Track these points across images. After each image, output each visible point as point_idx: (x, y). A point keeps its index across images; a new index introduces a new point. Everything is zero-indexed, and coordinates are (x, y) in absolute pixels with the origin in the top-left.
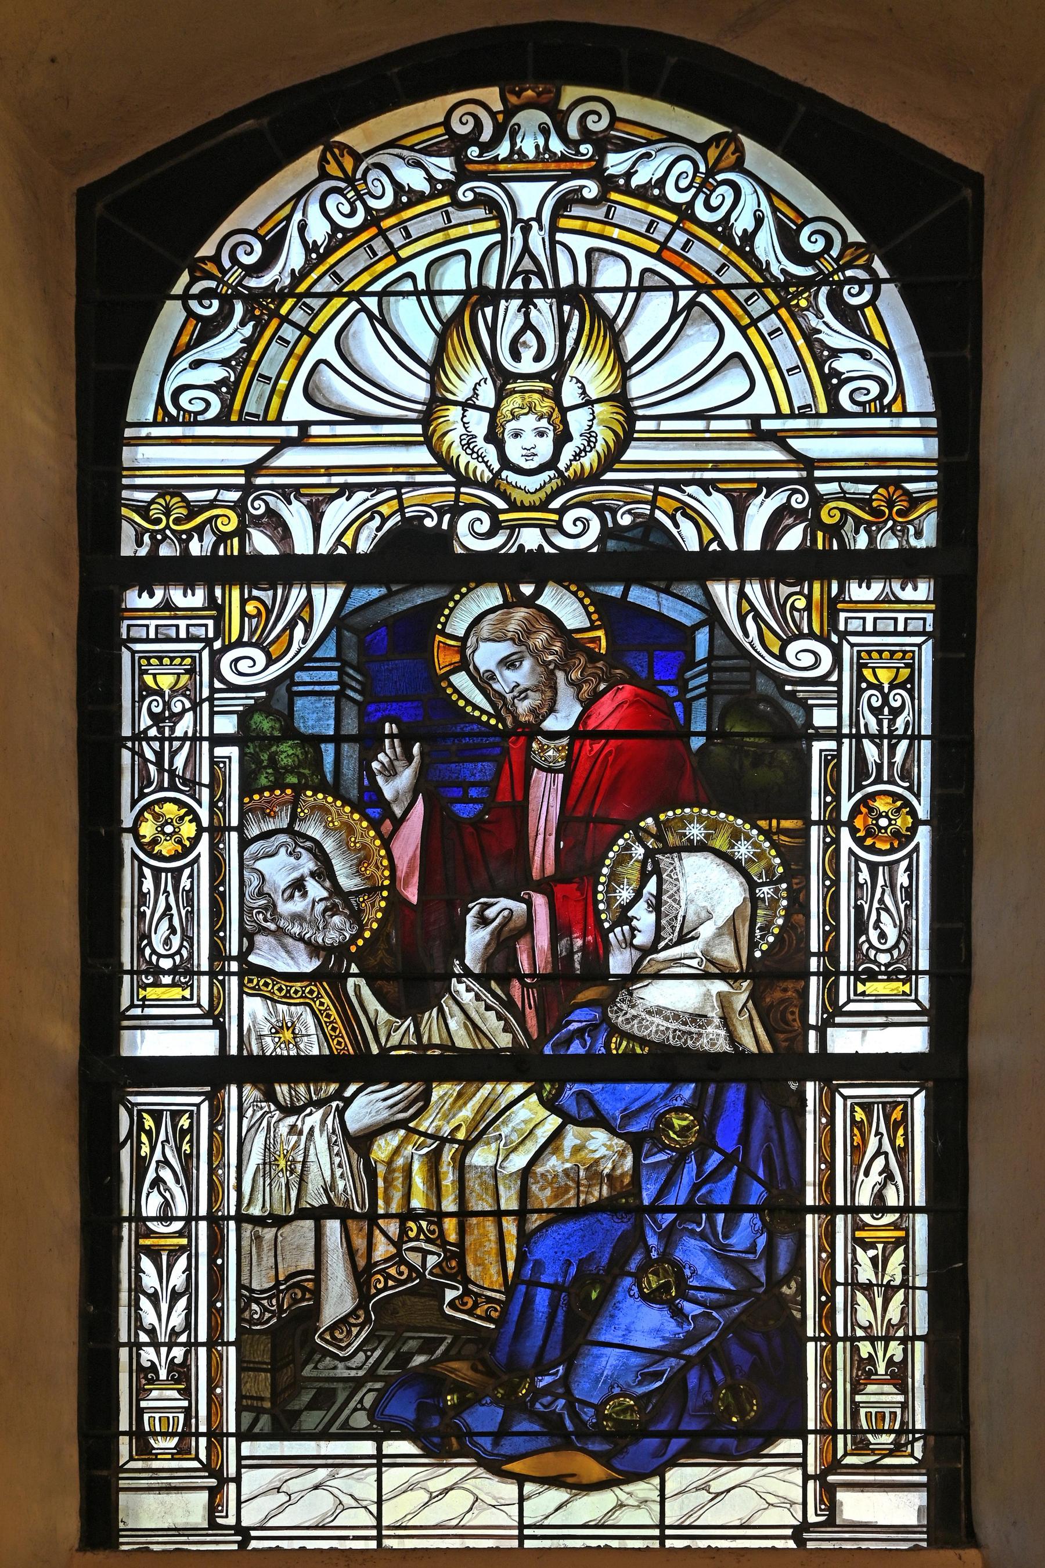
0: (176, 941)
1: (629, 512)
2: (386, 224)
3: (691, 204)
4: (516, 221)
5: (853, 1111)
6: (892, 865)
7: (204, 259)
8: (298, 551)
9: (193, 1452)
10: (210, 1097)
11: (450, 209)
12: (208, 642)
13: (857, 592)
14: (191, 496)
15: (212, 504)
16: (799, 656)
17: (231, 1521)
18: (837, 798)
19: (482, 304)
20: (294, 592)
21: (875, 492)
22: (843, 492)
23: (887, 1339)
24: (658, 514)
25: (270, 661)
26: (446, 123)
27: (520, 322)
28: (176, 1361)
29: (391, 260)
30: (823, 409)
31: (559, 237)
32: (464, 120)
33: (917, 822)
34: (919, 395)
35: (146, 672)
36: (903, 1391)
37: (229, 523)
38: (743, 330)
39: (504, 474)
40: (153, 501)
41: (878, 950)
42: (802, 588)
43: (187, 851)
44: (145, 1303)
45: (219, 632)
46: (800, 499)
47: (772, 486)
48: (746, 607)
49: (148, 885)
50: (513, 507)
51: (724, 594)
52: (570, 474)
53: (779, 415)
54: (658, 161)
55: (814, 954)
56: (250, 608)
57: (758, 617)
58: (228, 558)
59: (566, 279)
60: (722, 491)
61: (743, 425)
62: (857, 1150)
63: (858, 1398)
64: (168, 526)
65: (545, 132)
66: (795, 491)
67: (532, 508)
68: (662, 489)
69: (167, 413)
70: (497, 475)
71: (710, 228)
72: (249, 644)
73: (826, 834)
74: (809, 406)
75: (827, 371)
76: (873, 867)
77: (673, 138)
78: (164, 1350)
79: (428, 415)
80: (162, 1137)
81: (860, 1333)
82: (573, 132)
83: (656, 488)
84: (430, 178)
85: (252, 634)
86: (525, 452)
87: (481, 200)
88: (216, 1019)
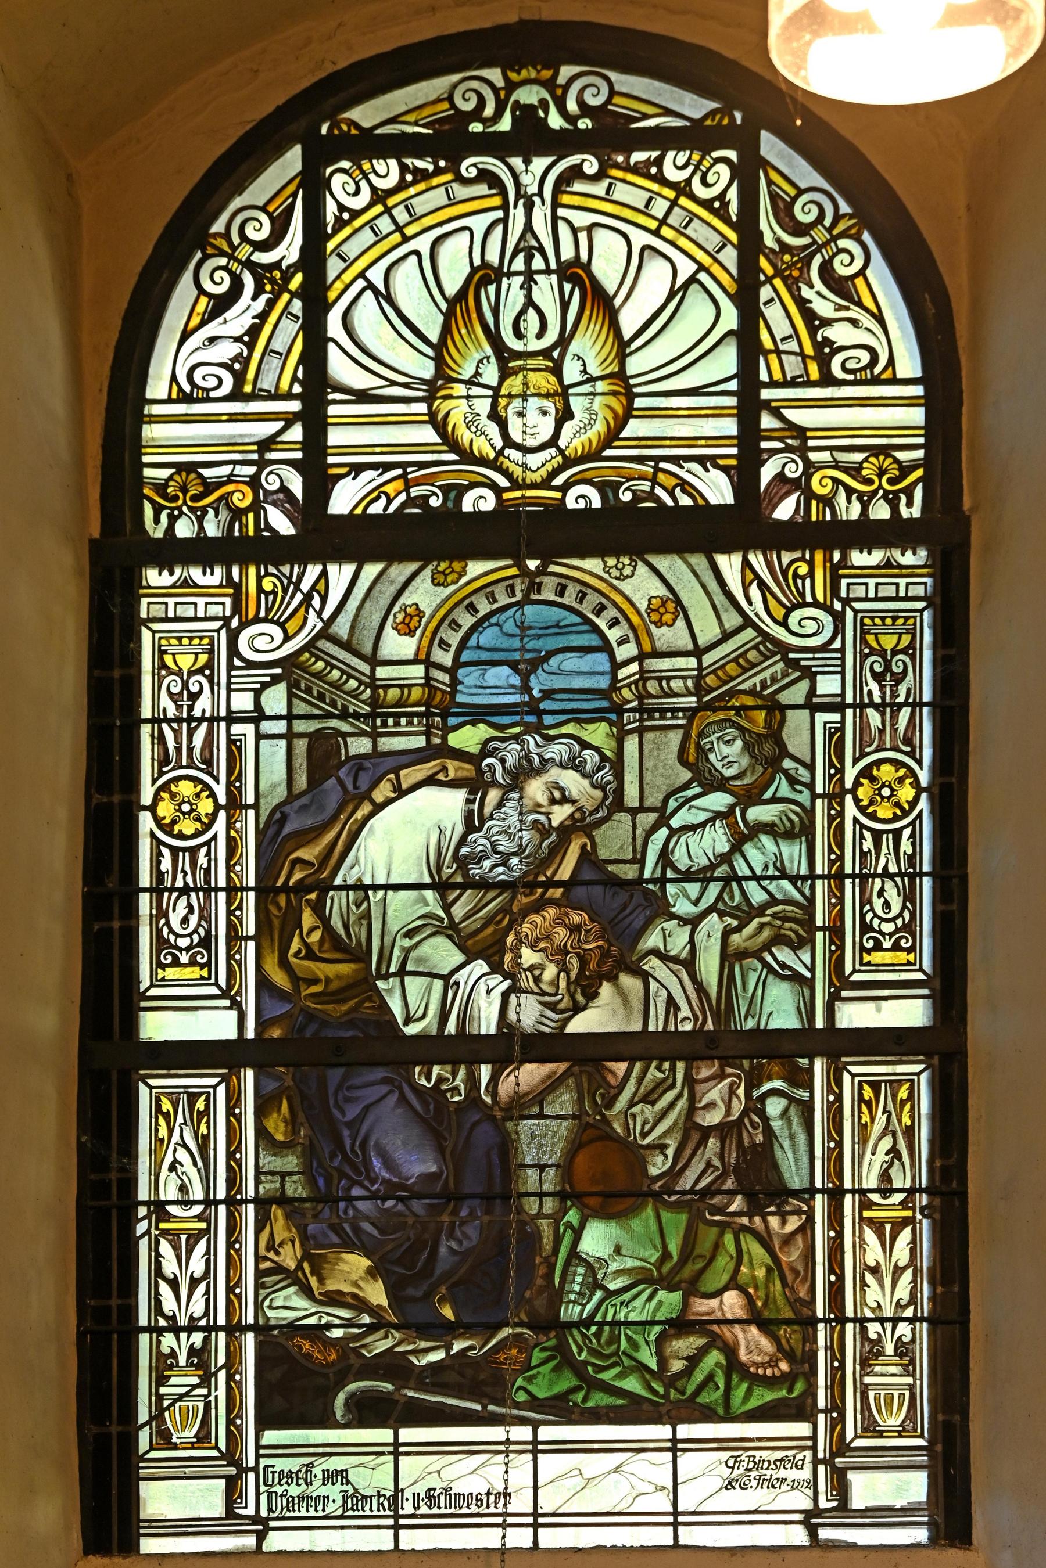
0: (194, 919)
2: (391, 202)
3: (688, 181)
4: (518, 195)
5: (861, 1088)
6: (897, 834)
7: (216, 235)
9: (213, 1441)
10: (224, 1078)
11: (454, 185)
13: (858, 558)
14: (206, 472)
15: (230, 479)
16: (803, 623)
17: (251, 1511)
18: (841, 771)
19: (485, 281)
20: (310, 567)
21: (866, 460)
22: (835, 460)
23: (895, 1321)
24: (658, 491)
25: (287, 638)
27: (521, 300)
31: (561, 212)
33: (152, 809)
35: (165, 652)
37: (242, 499)
39: (507, 452)
40: (171, 478)
41: (882, 920)
42: (804, 555)
43: (208, 827)
44: (164, 1289)
45: (237, 608)
48: (750, 576)
49: (166, 864)
50: (516, 485)
55: (820, 929)
56: (267, 584)
57: (762, 586)
59: (567, 253)
63: (868, 1380)
67: (534, 486)
68: (662, 465)
69: (180, 389)
70: (500, 453)
71: (707, 204)
72: (265, 620)
73: (831, 807)
75: (819, 339)
76: (877, 835)
78: (183, 1336)
79: (433, 389)
80: (180, 1119)
81: (869, 1314)
82: (572, 106)
83: (657, 464)
85: (268, 610)
87: (485, 176)
88: (233, 1000)
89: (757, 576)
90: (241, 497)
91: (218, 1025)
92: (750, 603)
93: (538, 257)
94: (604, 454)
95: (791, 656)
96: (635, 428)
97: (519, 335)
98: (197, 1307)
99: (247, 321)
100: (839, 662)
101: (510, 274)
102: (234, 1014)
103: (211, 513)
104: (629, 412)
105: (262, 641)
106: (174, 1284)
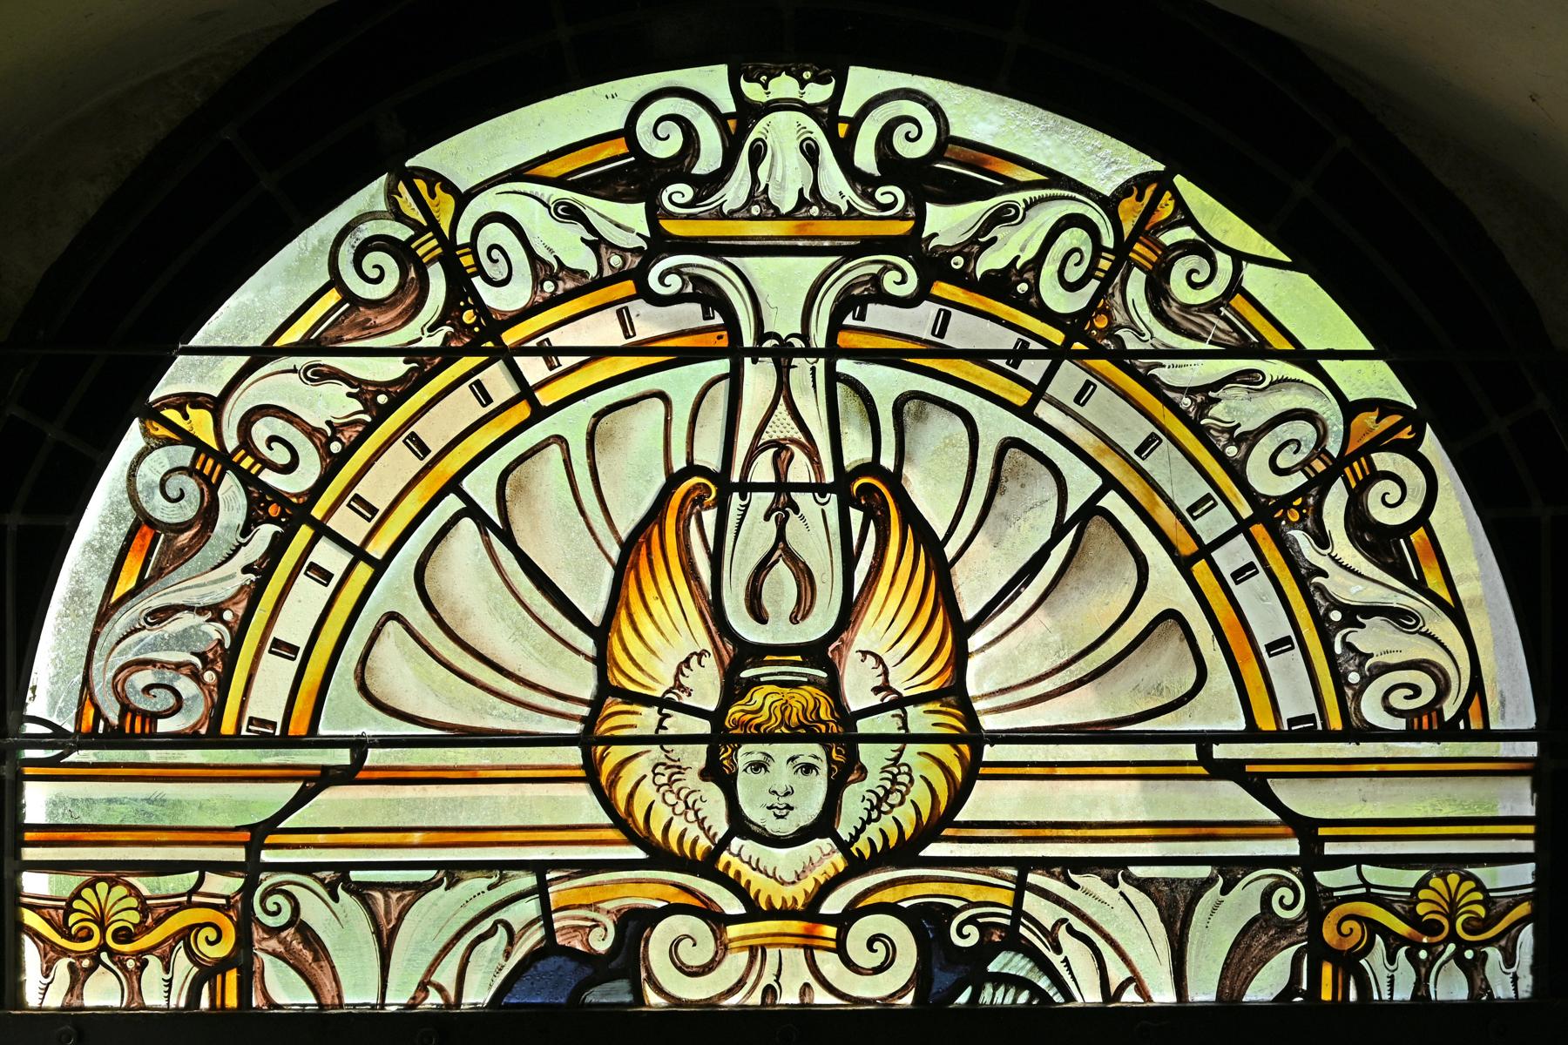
15: (189, 901)
21: (1423, 884)
26: (628, 132)
29: (523, 411)
30: (1336, 723)
38: (1184, 565)
47: (1231, 870)
50: (754, 912)
52: (862, 845)
53: (1252, 734)
58: (219, 1013)
59: (856, 450)
60: (1142, 885)
61: (1189, 752)
64: (103, 947)
66: (1282, 882)
68: (1032, 878)
74: (1311, 718)
82: (865, 157)
84: (597, 244)
86: (773, 800)
93: (800, 458)
94: (924, 853)
97: (759, 616)
101: (746, 488)
103: (154, 963)
104: (974, 770)
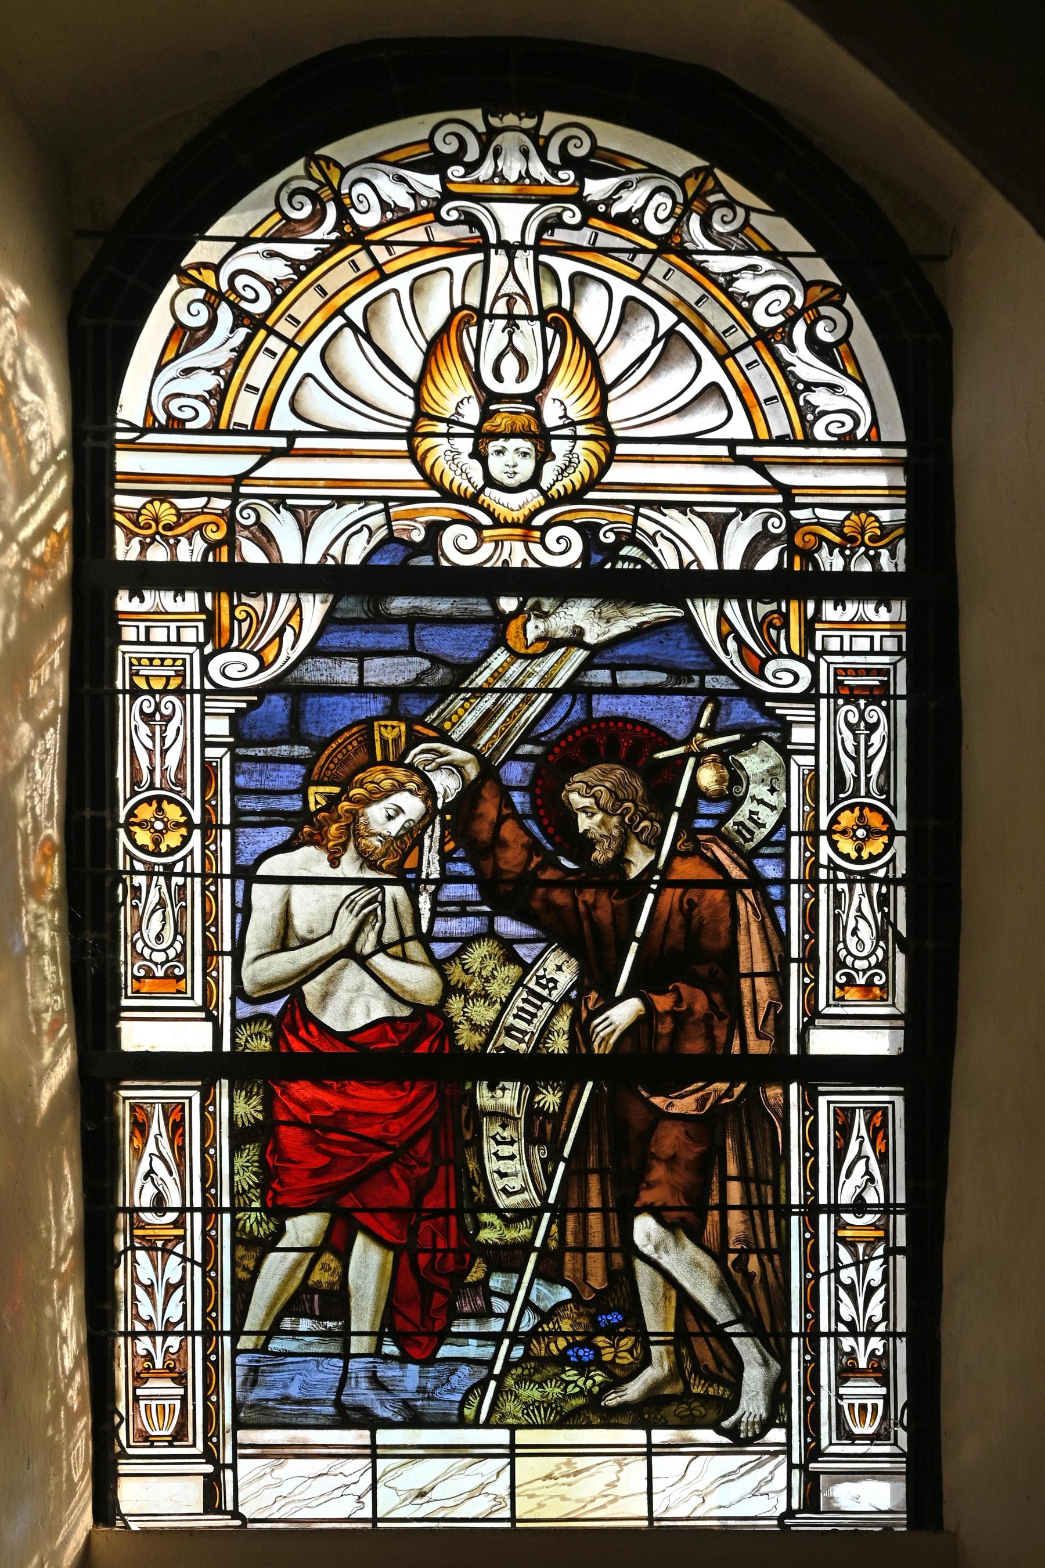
1: (611, 530)
8: (286, 560)
12: (200, 646)
14: (182, 503)
19: (466, 322)
20: (284, 597)
21: (847, 518)
25: (263, 668)
28: (171, 1350)
29: (376, 276)
32: (447, 140)
34: (894, 429)
36: (885, 1383)
38: (721, 360)
41: (856, 958)
42: (779, 606)
45: (209, 635)
46: (777, 524)
50: (497, 524)
51: (705, 615)
53: (756, 442)
54: (639, 192)
55: (794, 960)
57: (738, 638)
58: (217, 565)
62: (839, 1155)
64: (158, 532)
65: (525, 153)
72: (237, 649)
75: (802, 403)
77: (652, 169)
82: (554, 157)
84: (415, 196)
86: (507, 469)
89: (733, 630)
90: (215, 528)
91: (194, 1038)
92: (727, 652)
95: (768, 704)
96: (617, 473)
97: (498, 377)
98: (174, 1312)
99: (223, 356)
100: (813, 713)
101: (492, 317)
102: (209, 1025)
104: (612, 458)
105: (236, 667)
106: (149, 1289)
